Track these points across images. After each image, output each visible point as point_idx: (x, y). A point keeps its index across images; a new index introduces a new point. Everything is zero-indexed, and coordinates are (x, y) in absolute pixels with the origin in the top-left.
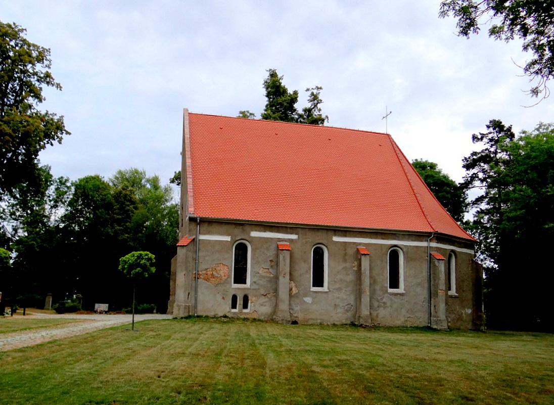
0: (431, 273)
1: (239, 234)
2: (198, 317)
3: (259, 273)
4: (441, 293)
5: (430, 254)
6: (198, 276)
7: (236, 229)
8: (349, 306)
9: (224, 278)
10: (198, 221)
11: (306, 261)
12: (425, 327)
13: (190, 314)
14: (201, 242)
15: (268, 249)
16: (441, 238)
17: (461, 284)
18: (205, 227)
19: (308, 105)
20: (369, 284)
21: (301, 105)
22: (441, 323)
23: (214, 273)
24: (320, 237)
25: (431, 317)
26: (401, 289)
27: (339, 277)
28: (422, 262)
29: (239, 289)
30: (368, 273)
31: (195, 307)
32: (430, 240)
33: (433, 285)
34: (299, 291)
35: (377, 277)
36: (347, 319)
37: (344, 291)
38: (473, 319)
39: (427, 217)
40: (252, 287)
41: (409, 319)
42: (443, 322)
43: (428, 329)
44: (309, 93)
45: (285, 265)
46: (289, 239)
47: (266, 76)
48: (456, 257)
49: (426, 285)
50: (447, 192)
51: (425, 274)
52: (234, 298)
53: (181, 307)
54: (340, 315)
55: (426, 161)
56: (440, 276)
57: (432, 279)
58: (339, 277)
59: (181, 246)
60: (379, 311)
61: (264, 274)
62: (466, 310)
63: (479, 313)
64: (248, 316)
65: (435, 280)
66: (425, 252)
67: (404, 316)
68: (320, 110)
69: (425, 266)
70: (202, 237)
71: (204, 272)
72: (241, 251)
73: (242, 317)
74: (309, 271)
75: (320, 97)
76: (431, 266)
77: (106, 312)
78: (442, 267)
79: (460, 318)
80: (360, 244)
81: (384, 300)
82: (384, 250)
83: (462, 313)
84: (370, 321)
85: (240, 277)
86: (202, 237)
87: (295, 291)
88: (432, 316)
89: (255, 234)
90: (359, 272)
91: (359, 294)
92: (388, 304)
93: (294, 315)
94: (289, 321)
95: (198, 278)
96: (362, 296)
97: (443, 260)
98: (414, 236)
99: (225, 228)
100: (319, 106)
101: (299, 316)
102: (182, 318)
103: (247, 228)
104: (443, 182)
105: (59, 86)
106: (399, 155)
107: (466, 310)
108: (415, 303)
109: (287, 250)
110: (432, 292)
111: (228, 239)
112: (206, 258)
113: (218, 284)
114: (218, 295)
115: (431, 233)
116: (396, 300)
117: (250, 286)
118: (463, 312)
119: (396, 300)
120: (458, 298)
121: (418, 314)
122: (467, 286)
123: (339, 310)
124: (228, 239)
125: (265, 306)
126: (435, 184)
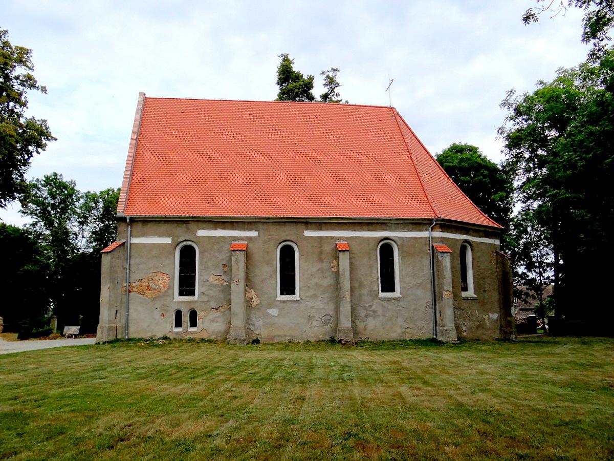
0: (435, 270)
1: (182, 234)
2: (129, 340)
3: (208, 281)
4: (447, 296)
5: (433, 247)
6: (130, 289)
7: (179, 229)
8: (328, 317)
9: (163, 290)
10: (128, 220)
11: (270, 262)
12: (429, 339)
13: (119, 337)
14: (132, 246)
15: (219, 251)
16: (447, 225)
17: (482, 282)
18: (138, 227)
19: (325, 90)
20: (349, 288)
21: (318, 90)
22: (448, 333)
23: (151, 284)
24: (287, 233)
25: (436, 326)
26: (397, 294)
27: (314, 281)
28: (422, 257)
29: (182, 302)
30: (348, 274)
31: (127, 327)
32: (432, 228)
33: (437, 285)
34: (261, 301)
35: (363, 279)
36: (325, 334)
37: (320, 299)
38: (501, 326)
39: (430, 201)
40: (200, 300)
41: (407, 330)
42: (450, 332)
43: (433, 342)
44: (324, 76)
45: (238, 269)
46: (247, 237)
47: (278, 62)
48: (472, 249)
49: (429, 286)
50: (485, 177)
51: (427, 271)
52: (179, 314)
53: (105, 329)
54: (316, 328)
55: (465, 145)
56: (445, 273)
57: (436, 278)
58: (314, 281)
59: (105, 253)
60: (367, 322)
61: (215, 283)
62: (490, 314)
63: (509, 319)
64: (195, 336)
65: (439, 279)
66: (426, 245)
67: (401, 326)
68: (338, 95)
69: (427, 262)
70: (135, 241)
71: (138, 284)
72: (188, 256)
73: (187, 337)
74: (273, 276)
75: (338, 79)
76: (435, 261)
77: (76, 336)
78: (446, 261)
79: (481, 325)
80: (340, 238)
81: (374, 308)
82: (372, 245)
83: (484, 319)
84: (352, 335)
85: (187, 286)
86: (135, 241)
87: (255, 301)
88: (438, 325)
89: (202, 233)
90: (337, 275)
91: (337, 300)
92: (380, 312)
93: (255, 332)
94: (244, 340)
95: (130, 292)
96: (341, 304)
97: (449, 252)
98: (411, 225)
99: (164, 228)
100: (336, 90)
101: (262, 333)
102: (104, 343)
103: (192, 226)
104: (479, 165)
105: (44, 90)
106: (400, 123)
107: (490, 314)
108: (415, 309)
109: (240, 250)
110: (436, 294)
111: (168, 240)
112: (141, 266)
113: (156, 298)
114: (156, 312)
115: (432, 220)
116: (390, 306)
117: (198, 298)
118: (486, 317)
119: (389, 307)
120: (477, 300)
121: (420, 324)
122: (489, 284)
123: (315, 323)
125: (217, 322)
126: (465, 171)
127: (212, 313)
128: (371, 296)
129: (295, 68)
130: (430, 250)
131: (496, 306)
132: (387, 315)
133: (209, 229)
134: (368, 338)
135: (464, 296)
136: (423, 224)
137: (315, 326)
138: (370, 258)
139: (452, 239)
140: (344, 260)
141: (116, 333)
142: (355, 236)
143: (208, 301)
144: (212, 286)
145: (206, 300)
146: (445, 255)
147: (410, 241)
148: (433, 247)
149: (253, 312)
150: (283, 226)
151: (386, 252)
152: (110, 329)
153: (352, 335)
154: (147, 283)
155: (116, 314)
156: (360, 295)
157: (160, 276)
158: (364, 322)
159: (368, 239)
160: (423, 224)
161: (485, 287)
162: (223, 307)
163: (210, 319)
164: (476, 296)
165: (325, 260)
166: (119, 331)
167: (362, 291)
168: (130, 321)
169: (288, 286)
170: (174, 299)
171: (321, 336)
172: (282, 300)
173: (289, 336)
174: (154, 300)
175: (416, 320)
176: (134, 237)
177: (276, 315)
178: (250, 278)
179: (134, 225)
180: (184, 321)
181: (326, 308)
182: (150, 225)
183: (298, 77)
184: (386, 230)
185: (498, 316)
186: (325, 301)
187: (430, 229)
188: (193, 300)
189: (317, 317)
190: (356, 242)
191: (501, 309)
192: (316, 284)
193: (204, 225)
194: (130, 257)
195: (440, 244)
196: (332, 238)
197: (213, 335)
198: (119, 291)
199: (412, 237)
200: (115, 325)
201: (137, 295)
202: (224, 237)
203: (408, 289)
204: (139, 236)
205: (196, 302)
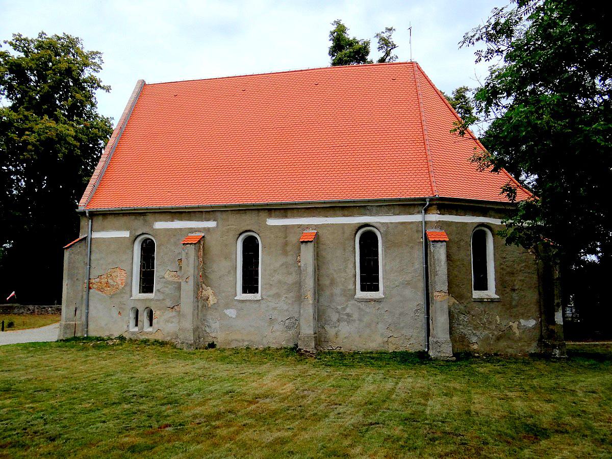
1: (139, 225)
3: (164, 278)
7: (136, 221)
8: (293, 320)
10: (87, 214)
11: (230, 256)
13: (79, 335)
14: (93, 241)
18: (99, 221)
19: (382, 54)
21: (374, 55)
24: (248, 222)
28: (412, 248)
37: (283, 298)
38: (541, 337)
41: (390, 340)
46: (204, 228)
49: (422, 285)
51: (419, 265)
54: (278, 333)
58: (277, 277)
61: (171, 279)
62: (522, 321)
63: (551, 327)
66: (417, 231)
67: (382, 335)
69: (419, 254)
70: (96, 235)
71: (98, 280)
72: (148, 250)
80: (308, 227)
82: (348, 232)
84: (313, 344)
85: (147, 285)
86: (96, 235)
87: (212, 300)
99: (123, 220)
103: (149, 218)
107: (522, 321)
109: (190, 244)
111: (126, 234)
112: (101, 262)
113: (114, 295)
115: (424, 199)
116: (370, 309)
119: (368, 310)
121: (407, 332)
123: (277, 327)
127: (167, 312)
128: (345, 296)
129: (350, 35)
131: (534, 309)
132: (365, 320)
133: (166, 221)
134: (341, 347)
136: (414, 205)
137: (278, 331)
138: (344, 250)
140: (307, 254)
142: (327, 223)
143: (163, 300)
144: (167, 282)
145: (161, 298)
146: (439, 245)
147: (396, 227)
148: (425, 234)
149: (209, 312)
150: (243, 215)
151: (369, 242)
152: (67, 327)
153: (314, 344)
155: (76, 311)
156: (332, 295)
157: (118, 273)
158: (335, 327)
159: (343, 226)
160: (414, 205)
161: (514, 285)
164: (498, 297)
165: (290, 253)
166: (79, 329)
167: (335, 290)
168: (89, 320)
169: (250, 285)
170: (131, 296)
171: (284, 343)
175: (403, 328)
176: (96, 231)
177: (234, 316)
178: (207, 274)
179: (95, 219)
181: (290, 309)
182: (110, 218)
184: (365, 215)
185: (536, 324)
186: (289, 302)
187: (423, 211)
190: (328, 230)
191: (541, 314)
192: (280, 282)
193: (162, 216)
194: (90, 252)
195: (438, 231)
196: (299, 226)
197: (168, 336)
198: (80, 288)
199: (399, 223)
200: (74, 323)
202: (181, 229)
203: (393, 288)
204: (99, 231)
205: (152, 300)
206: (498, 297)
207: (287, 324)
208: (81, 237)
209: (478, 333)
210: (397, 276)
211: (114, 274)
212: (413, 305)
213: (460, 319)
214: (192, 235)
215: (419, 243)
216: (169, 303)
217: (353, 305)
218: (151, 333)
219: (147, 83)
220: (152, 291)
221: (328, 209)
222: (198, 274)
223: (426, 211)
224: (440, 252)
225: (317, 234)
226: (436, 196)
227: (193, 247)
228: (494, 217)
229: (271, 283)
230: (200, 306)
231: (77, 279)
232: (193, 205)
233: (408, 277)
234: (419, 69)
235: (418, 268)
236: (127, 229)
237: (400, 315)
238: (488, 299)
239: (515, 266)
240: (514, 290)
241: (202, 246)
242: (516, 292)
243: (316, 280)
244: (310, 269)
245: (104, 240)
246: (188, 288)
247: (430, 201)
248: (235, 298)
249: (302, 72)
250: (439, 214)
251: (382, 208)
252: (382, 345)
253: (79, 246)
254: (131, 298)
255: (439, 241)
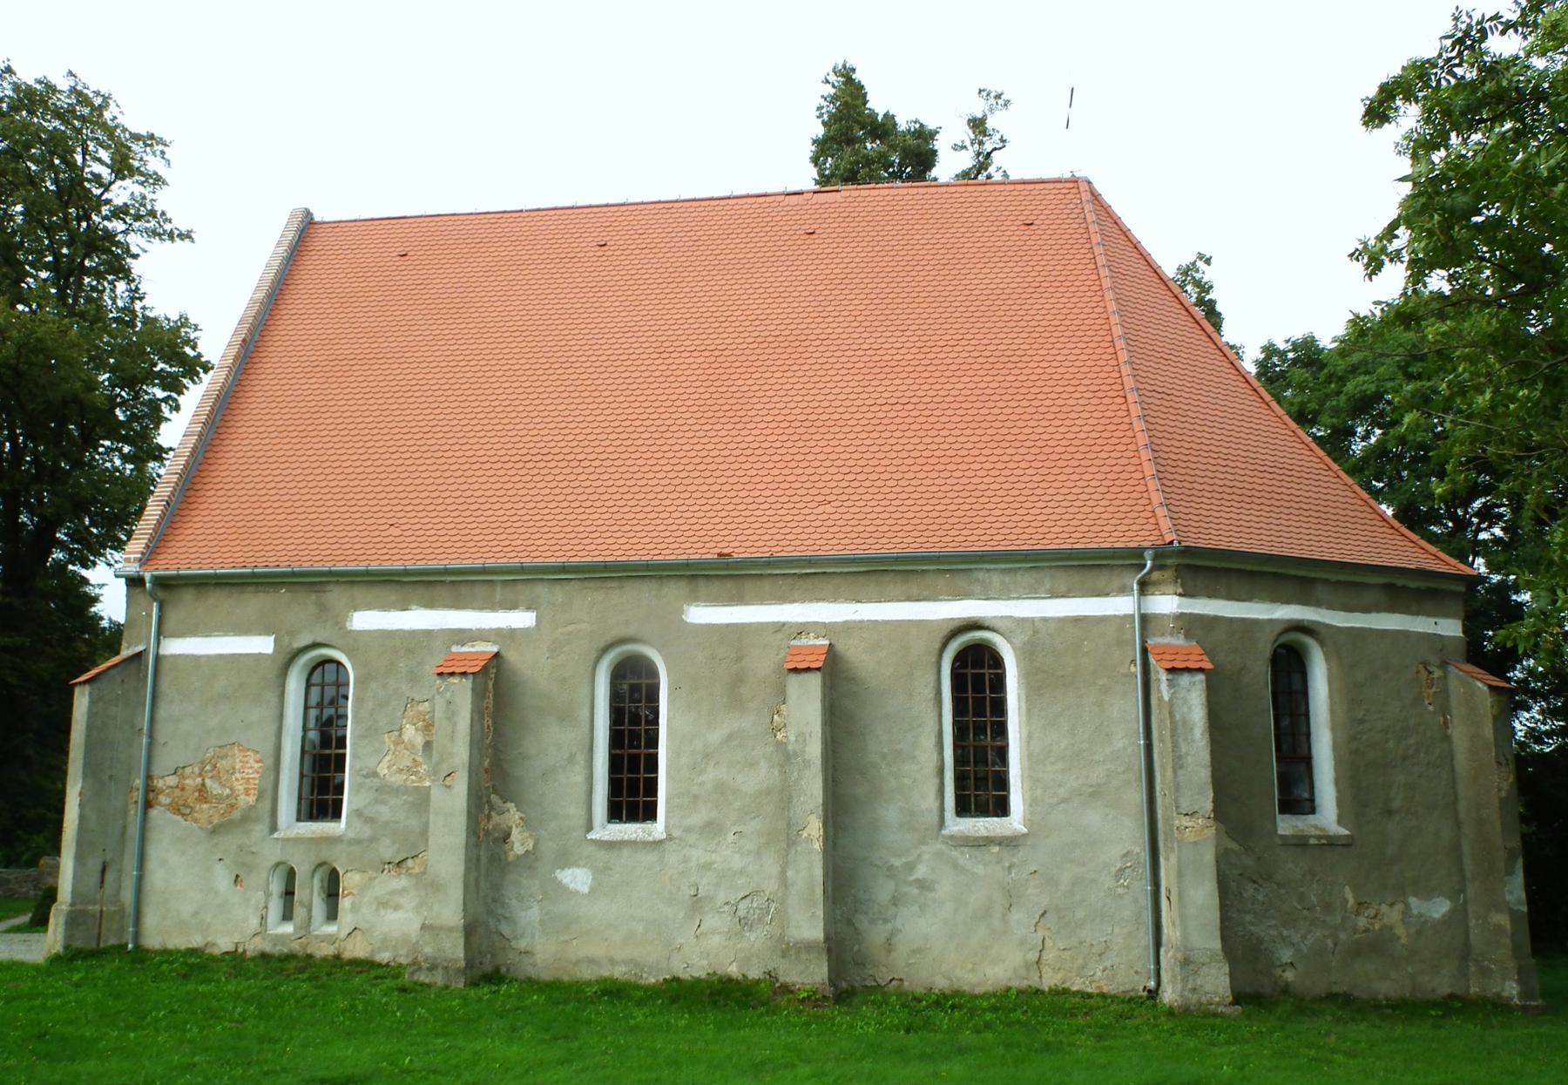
3: (375, 774)
14: (165, 667)
21: (949, 165)
23: (208, 782)
27: (712, 775)
37: (731, 837)
45: (452, 739)
49: (1138, 796)
51: (1125, 739)
54: (716, 940)
58: (712, 775)
59: (80, 683)
62: (1413, 901)
70: (175, 647)
80: (801, 630)
81: (921, 871)
86: (175, 647)
89: (365, 620)
97: (1201, 670)
99: (255, 603)
103: (336, 596)
107: (1413, 901)
108: (1077, 881)
111: (264, 645)
115: (1138, 553)
116: (981, 867)
124: (264, 645)
125: (397, 908)
129: (878, 104)
130: (1133, 661)
134: (901, 980)
135: (1287, 833)
139: (1231, 619)
141: (99, 934)
143: (373, 839)
154: (199, 780)
160: (249, 584)
162: (417, 860)
163: (376, 898)
170: (274, 828)
172: (606, 838)
173: (625, 963)
174: (215, 831)
180: (301, 903)
183: (883, 129)
185: (1452, 912)
188: (331, 832)
189: (721, 898)
196: (780, 627)
200: (97, 908)
201: (169, 815)
206: (1344, 831)
207: (741, 913)
208: (126, 652)
209: (1296, 938)
210: (1063, 771)
211: (222, 764)
212: (1113, 854)
213: (1245, 895)
214: (465, 649)
215: (1126, 676)
216: (387, 850)
217: (939, 854)
218: (331, 939)
219: (317, 218)
220: (337, 815)
221: (862, 579)
222: (481, 763)
223: (1144, 587)
224: (1192, 701)
225: (831, 652)
226: (1172, 542)
227: (467, 683)
228: (1331, 607)
229: (695, 790)
230: (484, 860)
231: (111, 777)
232: (467, 564)
233: (1097, 775)
234: (1096, 197)
235: (1125, 748)
236: (266, 631)
237: (1074, 884)
238: (1319, 838)
239: (1391, 744)
240: (1389, 813)
241: (491, 684)
242: (1397, 818)
243: (830, 780)
244: (815, 749)
245: (195, 660)
246: (452, 801)
247: (1155, 558)
248: (589, 836)
249: (768, 199)
250: (1180, 595)
251: (1019, 578)
252: (1022, 972)
253: (119, 679)
254: (275, 835)
255: (1188, 670)
